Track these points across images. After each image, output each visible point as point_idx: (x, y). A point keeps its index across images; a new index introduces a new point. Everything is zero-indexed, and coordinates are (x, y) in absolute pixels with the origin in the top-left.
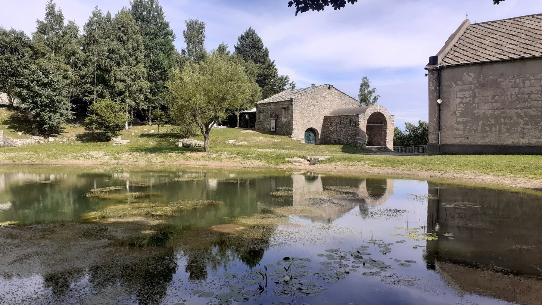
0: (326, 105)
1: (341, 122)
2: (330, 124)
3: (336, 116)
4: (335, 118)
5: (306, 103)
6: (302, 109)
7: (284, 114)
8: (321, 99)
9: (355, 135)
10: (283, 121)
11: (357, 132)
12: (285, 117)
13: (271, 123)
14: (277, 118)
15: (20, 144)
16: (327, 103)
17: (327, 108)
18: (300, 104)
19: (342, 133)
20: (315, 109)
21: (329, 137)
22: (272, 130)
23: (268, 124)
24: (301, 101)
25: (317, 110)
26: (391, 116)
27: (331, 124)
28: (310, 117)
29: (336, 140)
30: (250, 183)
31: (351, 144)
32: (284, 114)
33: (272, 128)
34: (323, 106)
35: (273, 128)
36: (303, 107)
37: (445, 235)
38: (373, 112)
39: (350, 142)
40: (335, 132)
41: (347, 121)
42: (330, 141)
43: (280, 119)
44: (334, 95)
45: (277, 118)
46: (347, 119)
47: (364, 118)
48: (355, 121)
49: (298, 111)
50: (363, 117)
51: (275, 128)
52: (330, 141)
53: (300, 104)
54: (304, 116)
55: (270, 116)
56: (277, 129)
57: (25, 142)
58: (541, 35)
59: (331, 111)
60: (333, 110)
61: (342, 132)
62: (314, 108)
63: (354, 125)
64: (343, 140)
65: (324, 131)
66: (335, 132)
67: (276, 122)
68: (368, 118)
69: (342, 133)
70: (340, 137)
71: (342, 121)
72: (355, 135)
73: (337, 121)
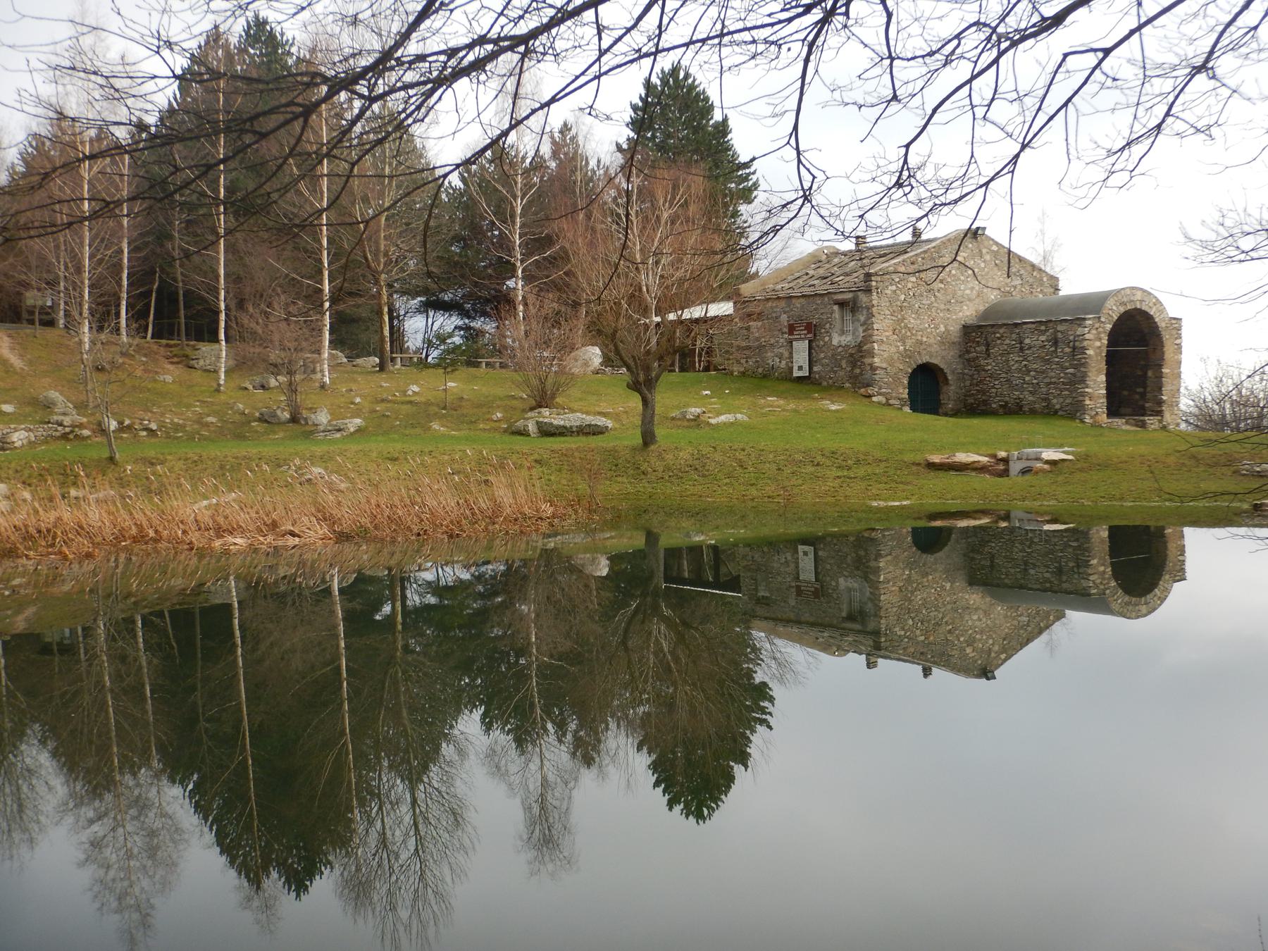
0: (968, 292)
1: (1021, 343)
2: (984, 348)
3: (1004, 325)
4: (1001, 331)
5: (910, 285)
6: (899, 303)
7: (838, 325)
8: (953, 272)
9: (1072, 383)
10: (835, 342)
11: (1079, 374)
12: (843, 332)
13: (791, 353)
14: (815, 335)
15: (20, 443)
16: (970, 285)
17: (970, 300)
18: (894, 288)
19: (1027, 379)
20: (935, 305)
21: (983, 392)
22: (796, 374)
23: (782, 354)
24: (897, 280)
25: (942, 307)
26: (1174, 322)
27: (987, 350)
28: (921, 330)
29: (1007, 399)
30: (744, 546)
31: (1060, 413)
32: (838, 325)
33: (795, 368)
34: (960, 293)
35: (800, 368)
36: (903, 297)
37: (762, 704)
38: (1122, 309)
39: (1058, 407)
40: (1004, 375)
41: (1043, 338)
42: (985, 402)
43: (827, 339)
44: (988, 257)
45: (815, 335)
46: (1043, 332)
47: (1101, 330)
48: (1071, 338)
49: (887, 312)
50: (1097, 325)
51: (806, 367)
52: (985, 402)
53: (894, 288)
54: (906, 327)
55: (786, 330)
56: (815, 369)
57: (31, 434)
58: (1256, 80)
59: (982, 308)
60: (987, 305)
61: (1028, 374)
62: (933, 299)
63: (1067, 350)
64: (1031, 398)
65: (964, 374)
66: (1004, 375)
67: (810, 348)
68: (1109, 327)
69: (1027, 379)
70: (1022, 390)
71: (1027, 341)
72: (1072, 383)
73: (1007, 341)
